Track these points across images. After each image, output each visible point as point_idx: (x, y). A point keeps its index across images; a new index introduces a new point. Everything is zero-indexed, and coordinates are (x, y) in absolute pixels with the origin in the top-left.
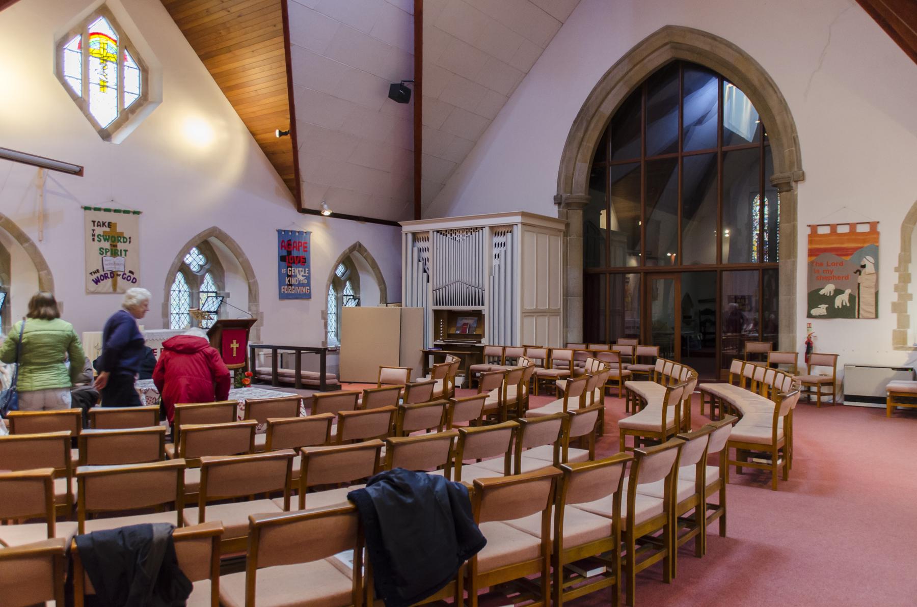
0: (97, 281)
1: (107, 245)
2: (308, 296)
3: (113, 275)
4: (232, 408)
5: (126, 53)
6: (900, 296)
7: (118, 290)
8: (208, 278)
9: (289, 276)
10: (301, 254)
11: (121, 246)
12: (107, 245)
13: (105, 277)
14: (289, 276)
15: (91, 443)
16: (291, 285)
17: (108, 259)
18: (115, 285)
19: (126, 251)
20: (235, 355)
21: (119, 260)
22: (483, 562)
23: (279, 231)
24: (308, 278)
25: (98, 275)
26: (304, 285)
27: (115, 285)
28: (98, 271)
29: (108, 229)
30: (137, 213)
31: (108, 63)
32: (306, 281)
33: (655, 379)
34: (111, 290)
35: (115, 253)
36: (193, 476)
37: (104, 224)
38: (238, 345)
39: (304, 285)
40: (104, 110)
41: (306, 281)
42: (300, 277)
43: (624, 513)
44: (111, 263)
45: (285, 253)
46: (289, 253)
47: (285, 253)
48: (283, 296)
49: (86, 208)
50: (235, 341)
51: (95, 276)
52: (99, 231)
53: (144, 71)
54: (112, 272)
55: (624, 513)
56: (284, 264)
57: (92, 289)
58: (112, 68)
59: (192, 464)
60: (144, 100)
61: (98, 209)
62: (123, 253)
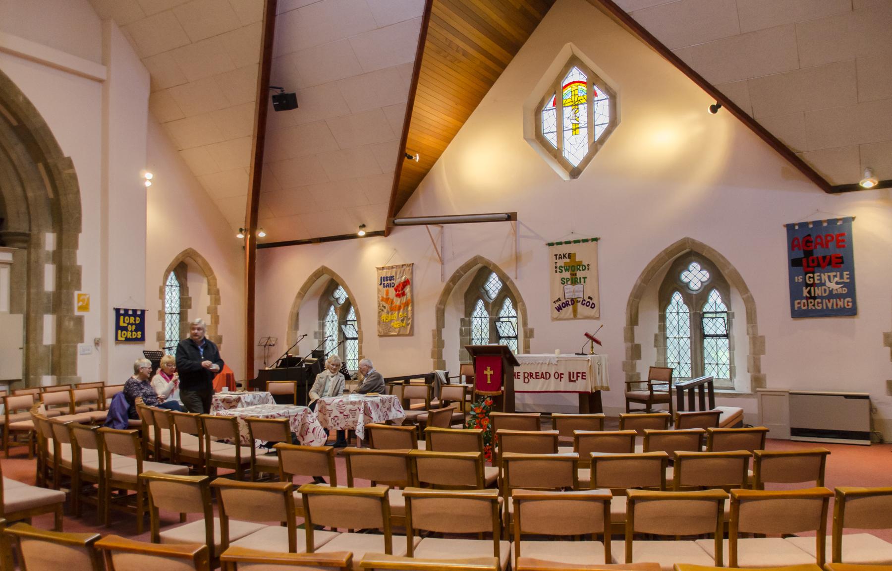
0: (559, 309)
1: (567, 275)
2: (852, 312)
3: (574, 301)
4: (818, 459)
5: (595, 88)
6: (633, 367)
7: (578, 316)
8: (715, 296)
9: (807, 285)
10: (832, 250)
11: (580, 274)
12: (567, 275)
13: (567, 304)
14: (807, 285)
15: (433, 436)
16: (814, 298)
17: (569, 288)
18: (575, 312)
19: (585, 278)
20: (489, 382)
21: (579, 287)
22: (201, 519)
23: (790, 227)
24: (851, 287)
25: (560, 303)
26: (840, 296)
27: (575, 312)
28: (559, 299)
29: (568, 260)
30: (596, 240)
31: (579, 106)
32: (845, 291)
33: (242, 424)
34: (572, 316)
35: (574, 281)
36: (619, 505)
37: (564, 256)
38: (492, 372)
39: (840, 296)
40: (575, 150)
41: (845, 291)
42: (832, 285)
43: (217, 521)
44: (571, 291)
45: (800, 254)
46: (808, 253)
47: (800, 254)
48: (797, 314)
49: (550, 244)
50: (489, 368)
51: (557, 305)
52: (561, 262)
53: (613, 97)
54: (572, 300)
55: (217, 521)
56: (800, 269)
57: (555, 316)
58: (583, 109)
59: (617, 492)
60: (614, 123)
61: (560, 243)
62: (582, 280)
